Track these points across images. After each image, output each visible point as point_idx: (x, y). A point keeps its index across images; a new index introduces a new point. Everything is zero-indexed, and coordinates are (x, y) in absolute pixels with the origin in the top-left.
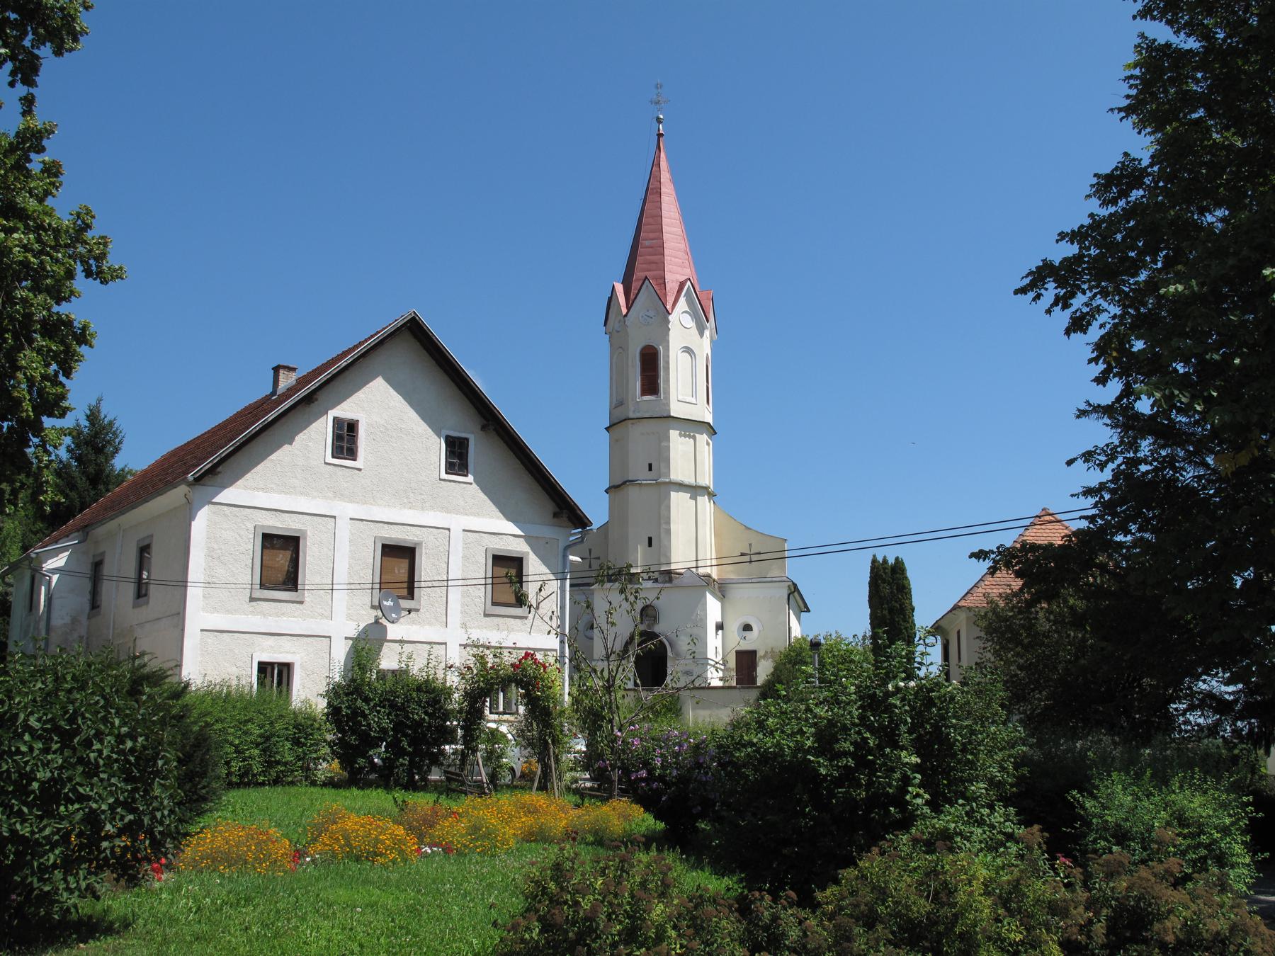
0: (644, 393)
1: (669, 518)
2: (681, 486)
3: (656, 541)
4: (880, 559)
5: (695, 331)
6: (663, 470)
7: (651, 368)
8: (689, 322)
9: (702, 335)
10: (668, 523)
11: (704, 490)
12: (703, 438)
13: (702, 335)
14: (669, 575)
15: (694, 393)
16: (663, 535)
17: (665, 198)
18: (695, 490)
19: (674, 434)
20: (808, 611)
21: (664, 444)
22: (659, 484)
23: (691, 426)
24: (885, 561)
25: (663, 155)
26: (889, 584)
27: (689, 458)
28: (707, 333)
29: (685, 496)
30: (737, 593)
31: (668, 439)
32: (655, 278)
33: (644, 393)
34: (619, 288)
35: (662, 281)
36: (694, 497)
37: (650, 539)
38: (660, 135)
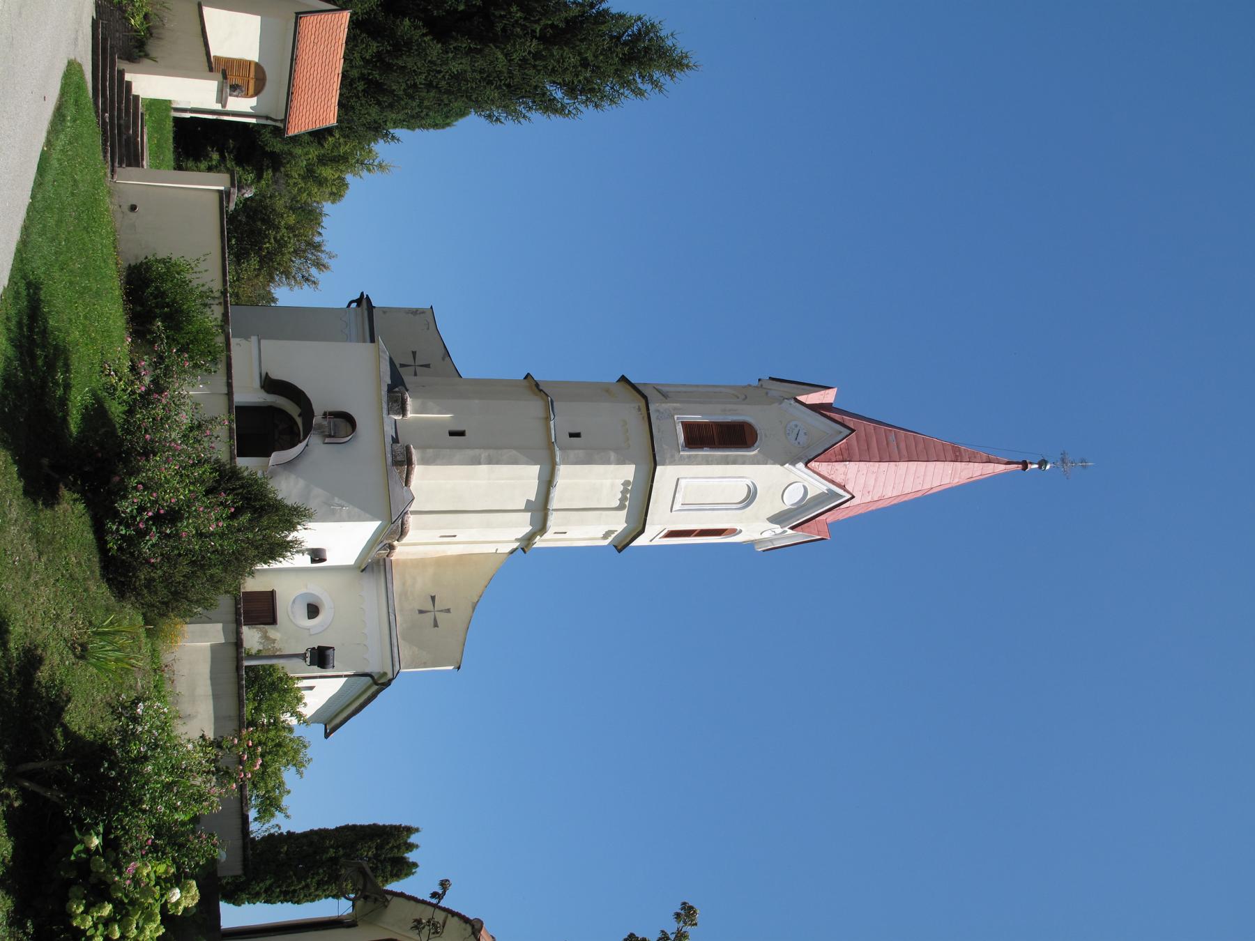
0: (688, 427)
1: (498, 462)
2: (547, 484)
3: (456, 441)
4: (413, 839)
5: (778, 508)
6: (572, 454)
7: (725, 438)
8: (793, 497)
9: (777, 519)
10: (490, 461)
11: (541, 527)
12: (618, 523)
13: (777, 519)
14: (403, 462)
15: (689, 507)
16: (470, 452)
17: (949, 467)
18: (540, 510)
19: (628, 472)
20: (327, 735)
21: (613, 455)
22: (550, 446)
23: (639, 503)
24: (411, 847)
25: (1001, 468)
26: (376, 856)
27: (590, 500)
28: (778, 529)
29: (530, 490)
30: (370, 592)
31: (621, 462)
32: (849, 447)
33: (688, 427)
34: (828, 397)
35: (846, 457)
36: (529, 507)
37: (462, 434)
38: (1025, 465)
